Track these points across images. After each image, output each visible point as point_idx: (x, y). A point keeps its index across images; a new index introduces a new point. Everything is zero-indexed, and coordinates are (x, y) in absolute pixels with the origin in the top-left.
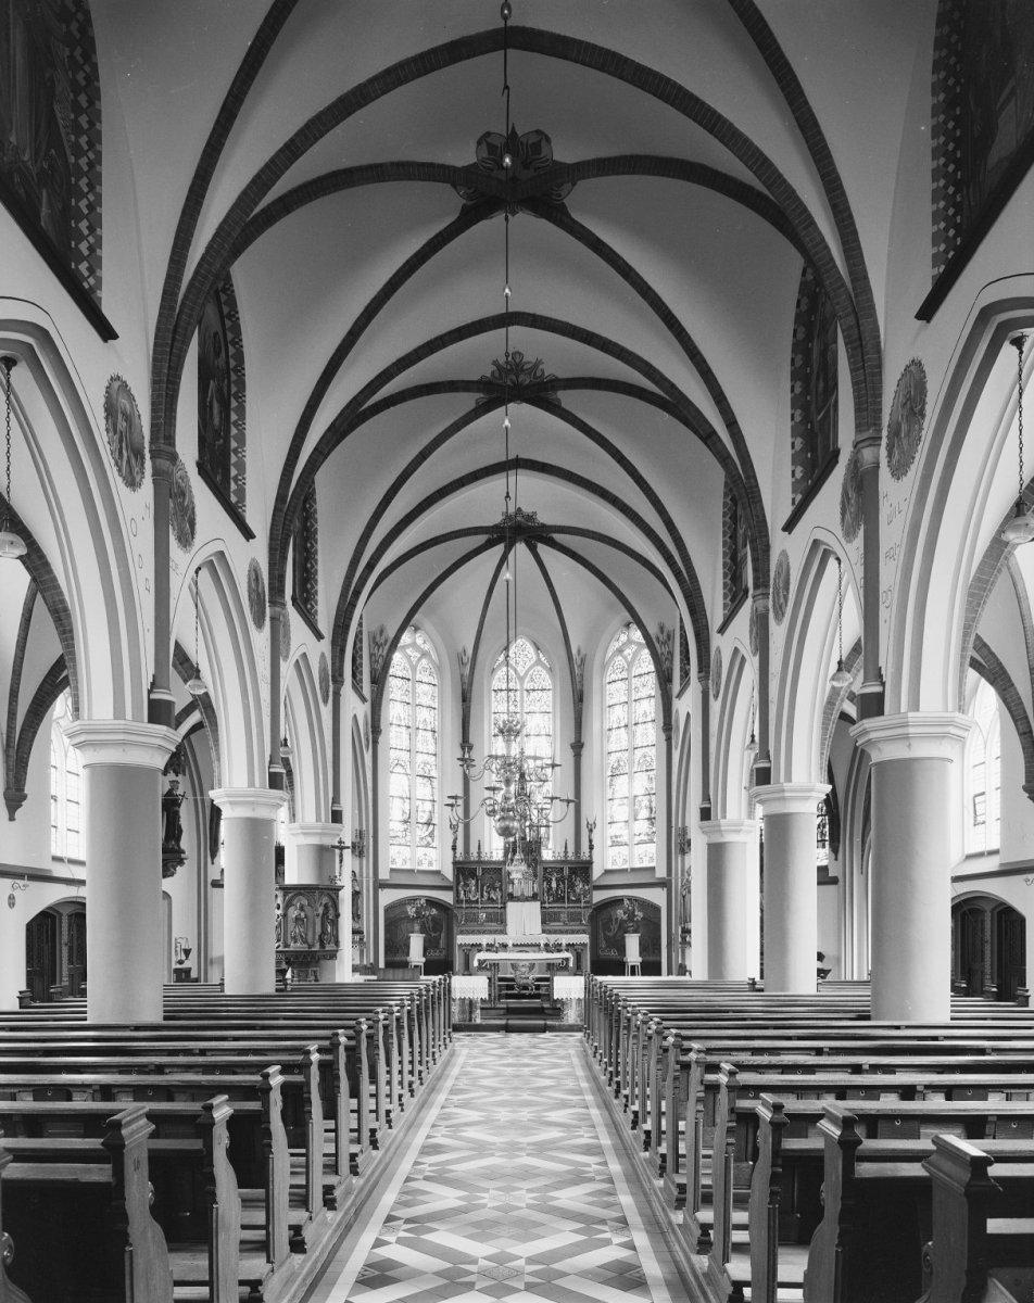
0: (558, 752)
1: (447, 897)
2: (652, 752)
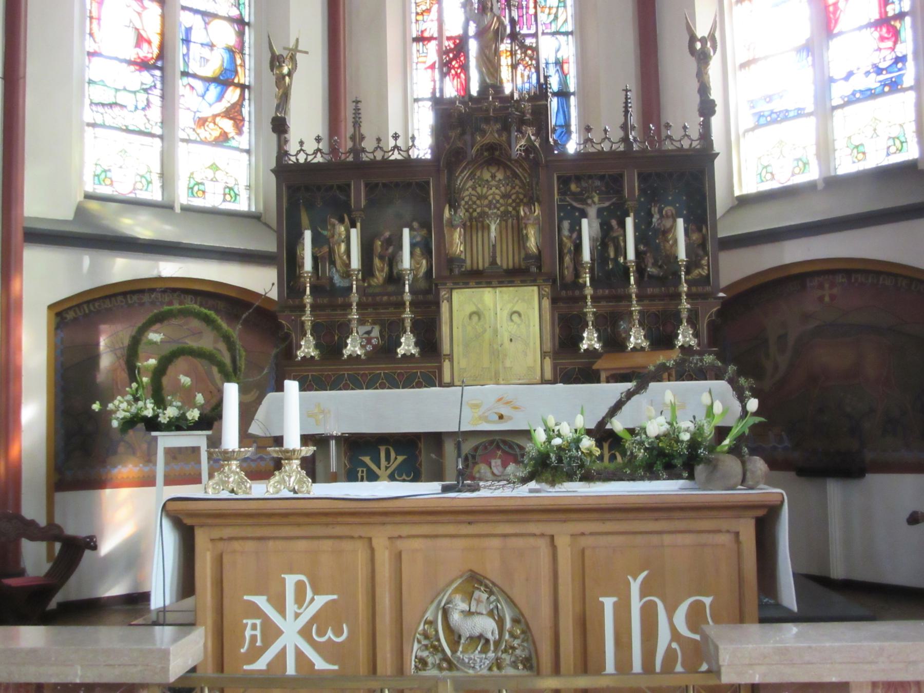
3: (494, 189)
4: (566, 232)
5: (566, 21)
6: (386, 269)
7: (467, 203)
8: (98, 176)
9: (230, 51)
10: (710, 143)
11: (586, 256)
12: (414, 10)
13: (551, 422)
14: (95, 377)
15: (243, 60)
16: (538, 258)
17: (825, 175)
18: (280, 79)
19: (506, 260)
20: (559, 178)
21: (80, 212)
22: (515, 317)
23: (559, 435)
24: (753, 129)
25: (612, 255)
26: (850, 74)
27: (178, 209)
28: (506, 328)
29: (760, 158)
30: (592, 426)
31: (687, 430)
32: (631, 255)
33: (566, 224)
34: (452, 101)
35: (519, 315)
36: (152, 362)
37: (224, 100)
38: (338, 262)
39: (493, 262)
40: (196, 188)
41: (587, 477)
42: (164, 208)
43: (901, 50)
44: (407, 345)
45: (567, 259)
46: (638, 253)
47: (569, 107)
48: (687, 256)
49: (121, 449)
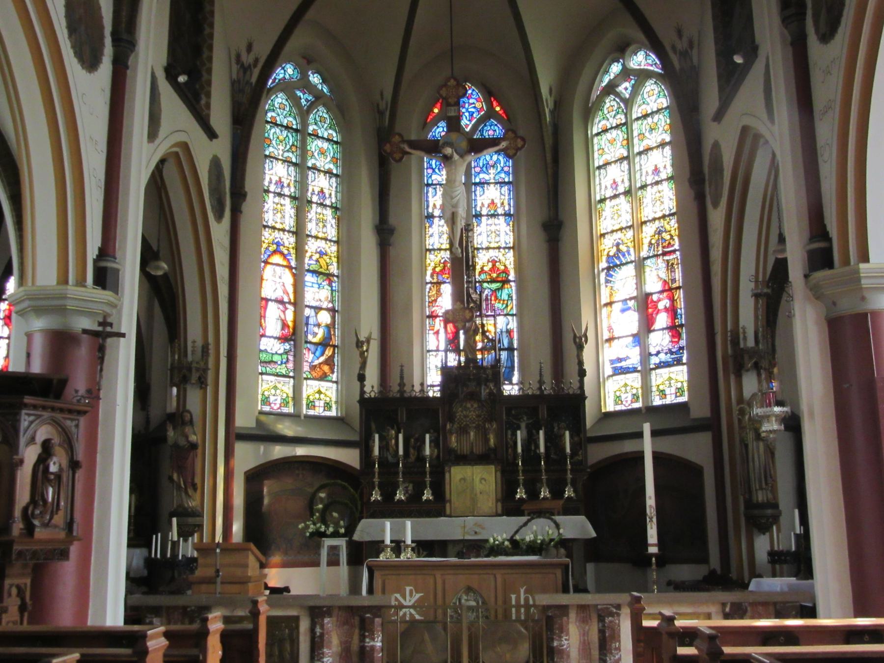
0: (524, 240)
1: (350, 457)
2: (672, 225)
3: (472, 412)
4: (510, 437)
5: (512, 308)
6: (416, 453)
7: (458, 419)
8: (263, 401)
9: (327, 326)
10: (584, 391)
11: (519, 450)
12: (427, 300)
13: (495, 535)
14: (261, 508)
15: (335, 332)
16: (494, 450)
17: (646, 405)
18: (362, 354)
19: (478, 449)
20: (506, 408)
21: (258, 422)
22: (483, 482)
23: (497, 541)
24: (612, 376)
25: (533, 448)
26: (658, 353)
27: (302, 418)
28: (478, 487)
29: (615, 392)
30: (509, 538)
31: (540, 539)
32: (542, 449)
33: (509, 432)
34: (451, 368)
35: (485, 480)
36: (320, 506)
37: (325, 355)
38: (391, 449)
39: (472, 452)
40: (311, 405)
41: (507, 554)
42: (295, 417)
43: (683, 343)
44: (427, 495)
45: (510, 450)
46: (546, 447)
47: (514, 356)
48: (571, 450)
49: (273, 547)
